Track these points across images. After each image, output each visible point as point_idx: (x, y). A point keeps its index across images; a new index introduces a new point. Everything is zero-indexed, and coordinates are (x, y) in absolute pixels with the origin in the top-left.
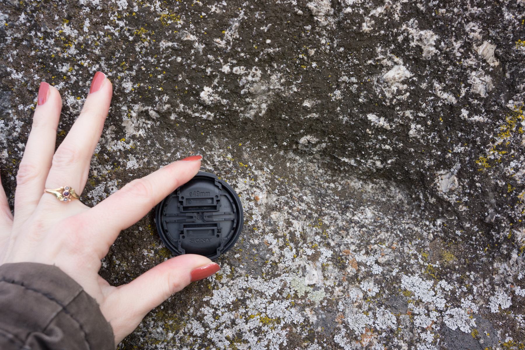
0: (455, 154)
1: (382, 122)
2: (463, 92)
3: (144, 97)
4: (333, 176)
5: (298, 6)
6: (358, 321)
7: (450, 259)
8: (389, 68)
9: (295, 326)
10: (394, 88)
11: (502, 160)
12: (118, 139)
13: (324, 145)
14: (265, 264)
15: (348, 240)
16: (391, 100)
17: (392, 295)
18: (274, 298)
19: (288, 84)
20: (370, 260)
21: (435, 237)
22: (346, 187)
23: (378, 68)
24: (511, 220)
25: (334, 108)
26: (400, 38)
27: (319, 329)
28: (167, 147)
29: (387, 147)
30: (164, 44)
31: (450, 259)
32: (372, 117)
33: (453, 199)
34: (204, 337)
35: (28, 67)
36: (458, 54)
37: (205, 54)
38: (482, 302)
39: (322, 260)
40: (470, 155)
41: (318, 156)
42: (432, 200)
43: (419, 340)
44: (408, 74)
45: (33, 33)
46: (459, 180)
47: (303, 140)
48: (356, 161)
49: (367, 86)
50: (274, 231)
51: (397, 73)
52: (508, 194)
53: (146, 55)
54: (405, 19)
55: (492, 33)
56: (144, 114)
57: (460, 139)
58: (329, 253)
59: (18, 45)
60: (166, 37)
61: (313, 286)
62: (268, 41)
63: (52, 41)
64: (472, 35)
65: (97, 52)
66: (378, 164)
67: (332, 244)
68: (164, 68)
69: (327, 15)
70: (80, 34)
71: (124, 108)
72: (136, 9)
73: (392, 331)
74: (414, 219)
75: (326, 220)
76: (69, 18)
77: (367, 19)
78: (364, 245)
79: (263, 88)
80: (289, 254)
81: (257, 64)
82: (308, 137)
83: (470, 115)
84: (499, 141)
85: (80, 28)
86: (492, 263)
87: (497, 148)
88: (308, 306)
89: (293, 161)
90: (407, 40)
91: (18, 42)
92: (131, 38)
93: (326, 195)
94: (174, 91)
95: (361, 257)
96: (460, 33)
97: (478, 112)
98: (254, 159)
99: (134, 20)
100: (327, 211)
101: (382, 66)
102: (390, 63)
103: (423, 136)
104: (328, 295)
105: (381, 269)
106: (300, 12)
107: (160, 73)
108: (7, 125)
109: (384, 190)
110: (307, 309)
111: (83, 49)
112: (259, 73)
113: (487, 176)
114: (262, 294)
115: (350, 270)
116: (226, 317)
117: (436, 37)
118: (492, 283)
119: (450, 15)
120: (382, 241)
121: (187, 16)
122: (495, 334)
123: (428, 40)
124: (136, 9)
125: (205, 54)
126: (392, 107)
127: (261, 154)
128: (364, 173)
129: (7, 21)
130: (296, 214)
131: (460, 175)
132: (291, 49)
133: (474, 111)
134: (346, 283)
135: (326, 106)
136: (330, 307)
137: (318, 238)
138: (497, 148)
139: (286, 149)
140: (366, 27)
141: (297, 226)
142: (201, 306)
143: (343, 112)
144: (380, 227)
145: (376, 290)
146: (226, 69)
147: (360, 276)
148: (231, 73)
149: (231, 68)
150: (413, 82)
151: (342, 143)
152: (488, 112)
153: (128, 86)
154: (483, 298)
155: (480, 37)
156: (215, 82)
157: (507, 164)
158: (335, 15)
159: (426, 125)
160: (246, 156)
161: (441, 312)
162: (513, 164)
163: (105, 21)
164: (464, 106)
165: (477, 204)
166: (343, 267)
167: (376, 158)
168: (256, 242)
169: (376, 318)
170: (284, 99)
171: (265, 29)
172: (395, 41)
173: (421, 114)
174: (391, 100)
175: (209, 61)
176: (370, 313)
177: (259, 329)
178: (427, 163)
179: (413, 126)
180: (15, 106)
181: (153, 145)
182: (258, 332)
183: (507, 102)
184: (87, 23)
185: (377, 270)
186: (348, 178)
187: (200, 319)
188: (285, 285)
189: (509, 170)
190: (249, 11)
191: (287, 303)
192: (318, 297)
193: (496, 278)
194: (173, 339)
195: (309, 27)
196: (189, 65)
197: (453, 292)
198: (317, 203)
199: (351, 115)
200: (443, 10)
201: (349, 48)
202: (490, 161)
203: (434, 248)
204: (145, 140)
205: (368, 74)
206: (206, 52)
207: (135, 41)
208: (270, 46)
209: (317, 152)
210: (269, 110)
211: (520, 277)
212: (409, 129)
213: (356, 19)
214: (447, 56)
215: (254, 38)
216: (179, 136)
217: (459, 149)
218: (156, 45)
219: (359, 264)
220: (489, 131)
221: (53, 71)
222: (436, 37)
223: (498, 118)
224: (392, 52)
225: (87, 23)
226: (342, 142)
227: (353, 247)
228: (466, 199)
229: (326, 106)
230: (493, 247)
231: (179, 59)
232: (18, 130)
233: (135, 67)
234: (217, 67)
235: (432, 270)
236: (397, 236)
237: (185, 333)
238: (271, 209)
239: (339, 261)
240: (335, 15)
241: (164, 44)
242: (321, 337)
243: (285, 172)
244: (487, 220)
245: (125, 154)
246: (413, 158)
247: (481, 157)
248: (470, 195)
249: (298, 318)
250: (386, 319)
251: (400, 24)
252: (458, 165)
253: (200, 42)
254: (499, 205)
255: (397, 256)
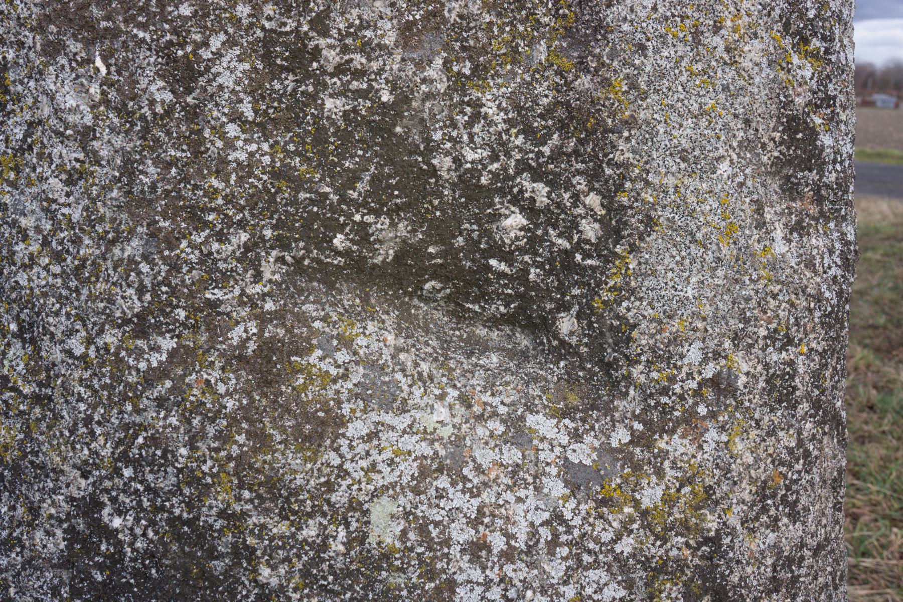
0: (573, 297)
1: (503, 267)
2: (576, 238)
3: (282, 243)
4: (457, 324)
5: (423, 162)
6: (485, 456)
7: (574, 400)
8: (507, 216)
9: (426, 458)
10: (512, 235)
11: (615, 300)
12: (256, 282)
13: (448, 291)
14: (395, 400)
15: (474, 382)
16: (510, 246)
17: (517, 432)
18: (404, 432)
19: (414, 231)
20: (496, 401)
21: (559, 379)
22: (471, 335)
23: (496, 217)
24: (627, 357)
25: (457, 254)
26: (515, 190)
27: (448, 461)
28: (300, 291)
29: (509, 291)
30: (302, 195)
31: (574, 400)
32: (493, 262)
33: (574, 340)
34: (340, 467)
35: (175, 215)
36: (568, 204)
37: (339, 205)
38: (603, 439)
39: (449, 399)
40: (586, 297)
41: (442, 303)
42: (555, 343)
43: (544, 473)
44: (525, 222)
45: (182, 185)
46: (578, 321)
47: (428, 286)
48: (480, 307)
49: (487, 233)
50: (403, 370)
51: (514, 221)
52: (623, 333)
53: (286, 205)
54: (518, 173)
55: (597, 185)
56: (281, 260)
57: (576, 282)
58: (456, 393)
59: (166, 196)
60: (305, 189)
61: (441, 422)
62: (396, 193)
63: (201, 193)
64: (578, 187)
65: (242, 202)
66: (502, 309)
67: (459, 385)
68: (301, 217)
69: (449, 170)
70: (227, 186)
71: (263, 254)
72: (278, 164)
73: (518, 465)
74: (539, 363)
75: (452, 364)
76: (218, 172)
77: (484, 173)
78: (489, 387)
79: (391, 235)
80: (418, 392)
81: (385, 213)
82: (433, 283)
83: (583, 259)
84: (611, 283)
85: (227, 181)
86: (612, 401)
87: (610, 290)
88: (437, 440)
89: (417, 308)
90: (521, 191)
91: (167, 193)
92: (273, 190)
93: (450, 342)
94: (309, 237)
95: (486, 398)
96: (568, 186)
97: (590, 256)
98: (381, 304)
99: (276, 174)
100: (453, 355)
101: (500, 215)
102: (507, 212)
103: (542, 280)
104: (456, 431)
105: (506, 409)
106: (425, 167)
107: (298, 221)
108: (152, 270)
109: (510, 337)
110: (436, 444)
111: (229, 200)
112: (387, 221)
113: (603, 317)
114: (393, 428)
115: (477, 409)
116: (361, 448)
117: (547, 189)
118: (613, 420)
119: (558, 170)
120: (507, 383)
121: (324, 171)
122: (615, 467)
123: (541, 192)
124: (278, 164)
125: (339, 205)
126: (511, 253)
127: (387, 300)
128: (488, 320)
129: (158, 174)
130: (423, 356)
131: (579, 317)
132: (417, 199)
133: (587, 255)
134: (472, 421)
135: (450, 252)
136: (458, 441)
137: (444, 379)
138: (610, 290)
139: (411, 295)
140: (484, 181)
141: (424, 367)
142: (337, 437)
143: (466, 257)
144: (505, 371)
145: (502, 428)
146: (357, 218)
147: (486, 415)
148: (362, 221)
149: (362, 217)
150: (530, 229)
151: (467, 286)
152: (599, 256)
153: (268, 233)
154: (604, 434)
155: (586, 189)
156: (347, 229)
157: (620, 304)
158: (456, 170)
159: (545, 269)
160: (373, 301)
161: (564, 447)
162: (624, 304)
163: (250, 174)
164: (577, 251)
165: (597, 348)
166: (469, 406)
167: (499, 302)
168: (387, 379)
169: (502, 453)
170: (411, 246)
171: (393, 181)
172: (511, 192)
173: (538, 259)
174: (510, 246)
175: (342, 210)
176: (497, 450)
177: (392, 460)
178: (548, 306)
179: (532, 270)
180: (161, 252)
181: (288, 288)
182: (391, 463)
183: (615, 246)
184: (233, 177)
185: (502, 410)
186: (473, 325)
187: (337, 450)
188: (415, 420)
189: (622, 310)
190: (379, 166)
191: (416, 438)
192: (446, 432)
193: (617, 415)
194: (312, 469)
195: (433, 180)
196: (324, 214)
197: (576, 429)
198: (442, 348)
199: (473, 261)
200: (552, 166)
201: (469, 199)
202: (604, 302)
203: (558, 390)
204: (281, 284)
205: (488, 222)
206: (340, 202)
207: (276, 193)
208: (397, 197)
209: (442, 298)
210: (396, 257)
211: (637, 412)
212: (529, 273)
213: (475, 173)
214: (559, 205)
215: (384, 190)
216: (311, 280)
217: (576, 291)
218: (296, 196)
219: (485, 404)
220: (602, 274)
221: (200, 219)
222: (547, 189)
223: (609, 262)
224: (509, 202)
225: (234, 177)
226: (465, 287)
227: (478, 388)
228: (586, 340)
229: (450, 252)
230: (613, 386)
231: (315, 209)
232: (163, 274)
233: (276, 216)
234: (349, 216)
235: (556, 410)
236: (522, 378)
237: (322, 464)
238: (399, 350)
239: (465, 401)
240: (456, 170)
241: (302, 195)
242: (449, 470)
243: (410, 319)
244: (606, 360)
245: (263, 296)
246: (534, 302)
247: (596, 298)
248: (589, 336)
249: (429, 452)
250: (512, 455)
251: (514, 178)
252: (577, 307)
253: (335, 193)
254: (616, 345)
255: (521, 397)
